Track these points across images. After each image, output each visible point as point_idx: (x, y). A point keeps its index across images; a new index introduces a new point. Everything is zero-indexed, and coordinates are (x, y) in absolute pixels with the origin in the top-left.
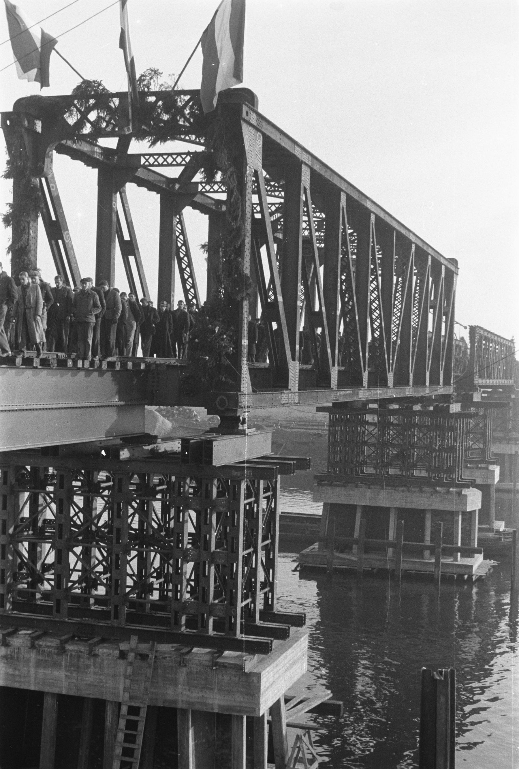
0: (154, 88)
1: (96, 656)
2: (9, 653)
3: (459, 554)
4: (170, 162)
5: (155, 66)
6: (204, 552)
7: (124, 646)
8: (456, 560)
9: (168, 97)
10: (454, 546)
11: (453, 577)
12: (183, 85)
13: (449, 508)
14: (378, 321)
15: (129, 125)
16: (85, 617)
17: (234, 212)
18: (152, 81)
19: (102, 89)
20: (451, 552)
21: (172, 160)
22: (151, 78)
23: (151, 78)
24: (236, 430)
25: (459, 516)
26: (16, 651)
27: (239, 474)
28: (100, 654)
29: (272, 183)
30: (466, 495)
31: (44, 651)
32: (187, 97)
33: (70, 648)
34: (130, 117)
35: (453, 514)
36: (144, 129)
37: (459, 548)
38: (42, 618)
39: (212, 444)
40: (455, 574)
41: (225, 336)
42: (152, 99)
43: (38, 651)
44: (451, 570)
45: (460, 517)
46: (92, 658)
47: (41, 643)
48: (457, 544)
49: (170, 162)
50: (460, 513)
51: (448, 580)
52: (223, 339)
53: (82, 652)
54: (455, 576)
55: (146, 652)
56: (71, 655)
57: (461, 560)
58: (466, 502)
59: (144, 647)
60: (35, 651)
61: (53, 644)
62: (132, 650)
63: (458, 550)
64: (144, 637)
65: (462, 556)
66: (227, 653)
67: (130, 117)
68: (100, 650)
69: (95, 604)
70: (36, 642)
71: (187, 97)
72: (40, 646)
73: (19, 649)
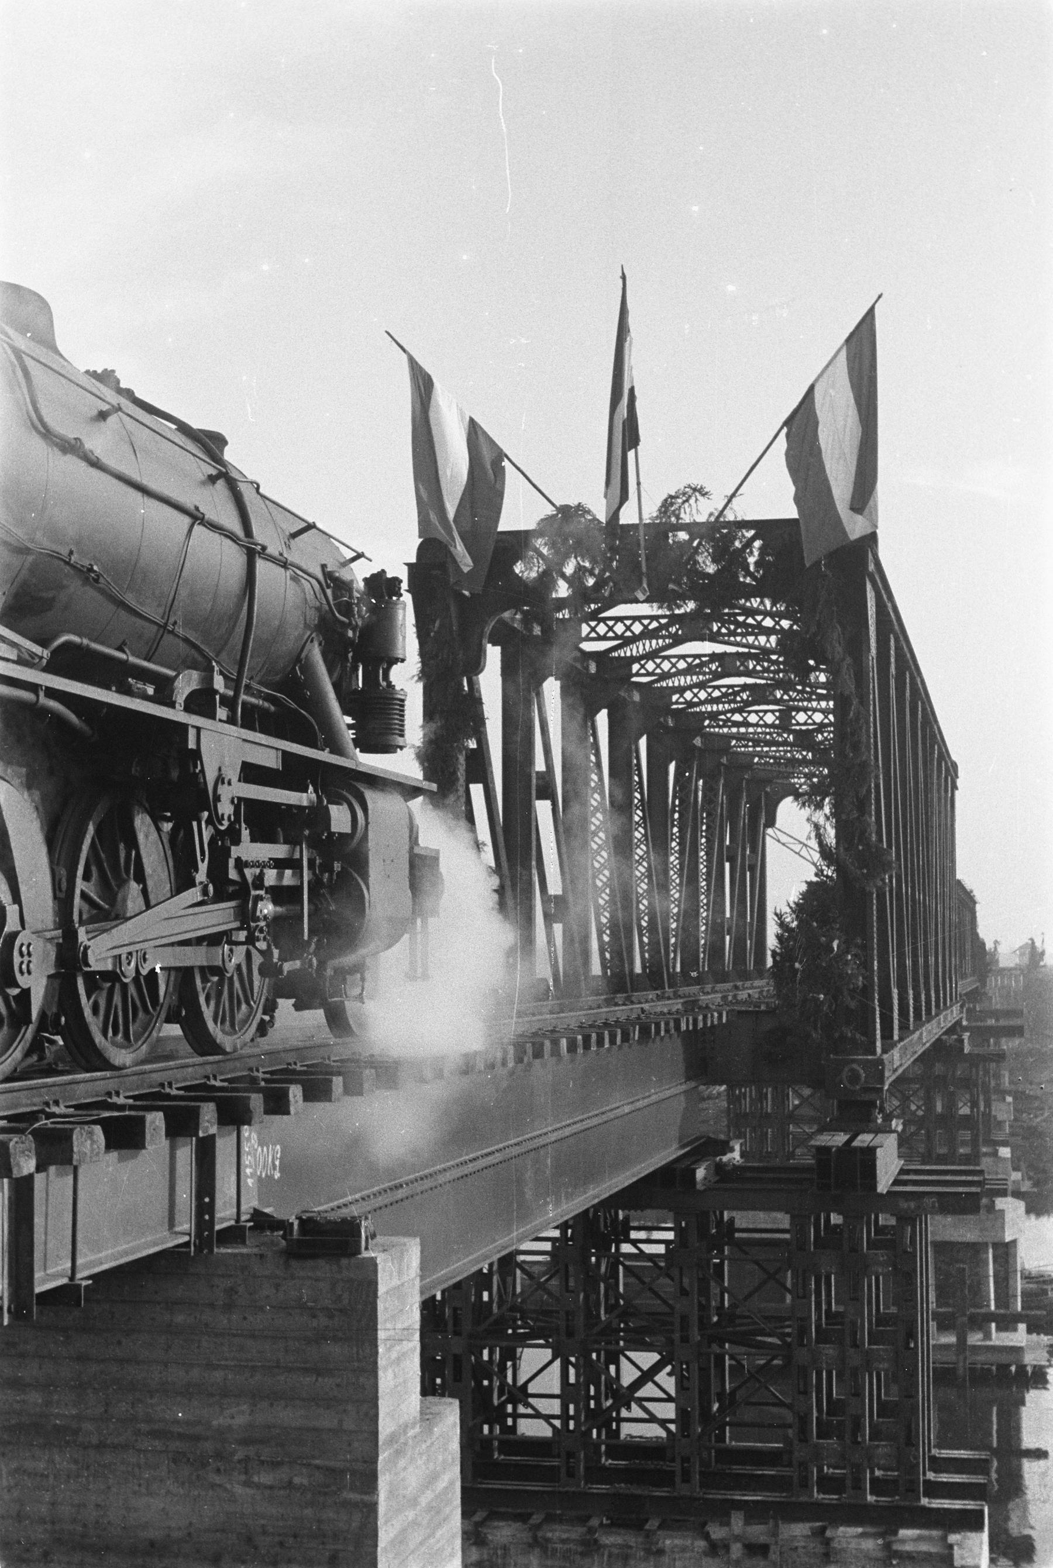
0: (686, 518)
1: (661, 1552)
2: (485, 1557)
3: (993, 1325)
4: (602, 634)
5: (696, 482)
6: (852, 1350)
7: (717, 1532)
8: (988, 1336)
9: (720, 534)
10: (983, 1311)
11: (989, 1370)
12: (746, 509)
13: (970, 1236)
14: (645, 864)
15: (641, 583)
16: (619, 1483)
17: (853, 734)
18: (686, 505)
19: (590, 520)
20: (980, 1322)
21: (606, 629)
22: (684, 502)
23: (684, 502)
24: (871, 1125)
25: (987, 1253)
26: (499, 1552)
27: (912, 1205)
28: (667, 1549)
29: (774, 657)
30: (1003, 1211)
31: (554, 1550)
32: (750, 534)
33: (607, 1542)
34: (644, 569)
35: (976, 1249)
36: (673, 590)
37: (992, 1314)
38: (536, 1488)
39: (875, 1154)
40: (992, 1365)
41: (849, 957)
42: (683, 536)
43: (544, 1550)
44: (981, 1358)
45: (991, 1251)
46: (652, 1558)
47: (549, 1535)
48: (988, 1306)
49: (602, 634)
50: (990, 1246)
51: (980, 1377)
52: (847, 963)
53: (631, 1547)
54: (994, 1368)
55: (763, 1539)
56: (610, 1556)
57: (999, 1338)
58: (1003, 1224)
59: (758, 1532)
60: (537, 1551)
61: (574, 1536)
62: (737, 1538)
63: (990, 1317)
64: (755, 1513)
65: (998, 1329)
66: (904, 1533)
67: (644, 569)
68: (668, 1542)
69: (609, 1455)
70: (540, 1534)
71: (750, 534)
72: (548, 1540)
73: (505, 1548)
